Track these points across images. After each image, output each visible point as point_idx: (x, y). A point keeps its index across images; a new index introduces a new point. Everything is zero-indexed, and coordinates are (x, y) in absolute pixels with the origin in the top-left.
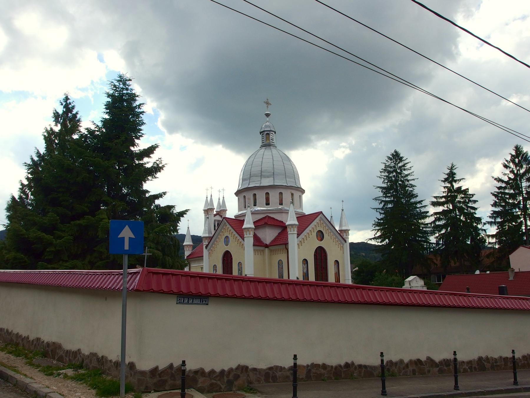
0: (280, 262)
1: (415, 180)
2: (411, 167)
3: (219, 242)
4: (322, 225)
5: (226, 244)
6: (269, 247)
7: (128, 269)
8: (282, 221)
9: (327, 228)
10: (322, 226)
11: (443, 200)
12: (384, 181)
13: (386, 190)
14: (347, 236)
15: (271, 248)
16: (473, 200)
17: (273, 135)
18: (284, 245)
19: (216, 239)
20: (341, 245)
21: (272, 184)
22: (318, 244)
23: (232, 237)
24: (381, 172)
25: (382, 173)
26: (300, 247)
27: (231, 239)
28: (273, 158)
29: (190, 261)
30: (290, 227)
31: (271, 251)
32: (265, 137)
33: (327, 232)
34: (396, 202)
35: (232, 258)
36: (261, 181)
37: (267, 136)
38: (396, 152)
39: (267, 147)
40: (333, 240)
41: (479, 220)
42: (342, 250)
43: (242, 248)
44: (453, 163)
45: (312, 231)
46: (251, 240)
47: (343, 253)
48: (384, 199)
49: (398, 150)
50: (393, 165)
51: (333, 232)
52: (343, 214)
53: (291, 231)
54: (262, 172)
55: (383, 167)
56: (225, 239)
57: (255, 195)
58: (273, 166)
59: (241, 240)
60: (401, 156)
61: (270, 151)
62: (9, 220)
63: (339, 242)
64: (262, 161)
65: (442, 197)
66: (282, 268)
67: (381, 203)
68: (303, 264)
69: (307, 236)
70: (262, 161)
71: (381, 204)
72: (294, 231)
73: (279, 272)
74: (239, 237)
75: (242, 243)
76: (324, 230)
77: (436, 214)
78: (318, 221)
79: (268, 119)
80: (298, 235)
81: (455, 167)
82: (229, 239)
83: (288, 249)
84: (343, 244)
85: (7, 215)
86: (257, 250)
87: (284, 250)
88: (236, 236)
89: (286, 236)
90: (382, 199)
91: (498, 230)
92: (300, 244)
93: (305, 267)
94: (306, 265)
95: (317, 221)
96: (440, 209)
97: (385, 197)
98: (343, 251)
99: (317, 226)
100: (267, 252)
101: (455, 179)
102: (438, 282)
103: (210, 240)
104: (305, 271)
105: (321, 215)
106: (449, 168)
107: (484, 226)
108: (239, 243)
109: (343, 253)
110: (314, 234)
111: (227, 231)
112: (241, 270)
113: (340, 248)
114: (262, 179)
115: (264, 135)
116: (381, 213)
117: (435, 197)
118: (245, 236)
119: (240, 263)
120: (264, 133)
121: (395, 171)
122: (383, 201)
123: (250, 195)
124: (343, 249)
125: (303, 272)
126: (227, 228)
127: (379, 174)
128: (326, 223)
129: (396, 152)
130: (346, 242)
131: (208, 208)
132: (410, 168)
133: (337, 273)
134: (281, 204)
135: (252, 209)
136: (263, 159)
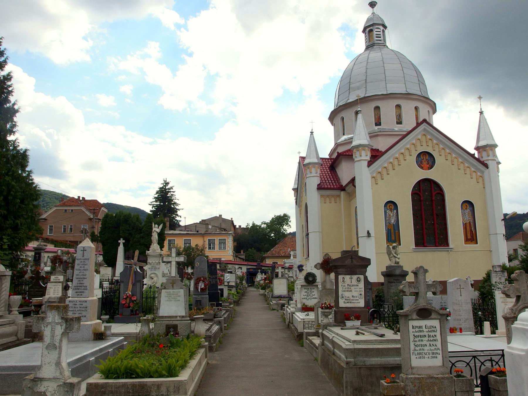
7: (400, 348)
14: (488, 156)
20: (479, 174)
26: (380, 182)
51: (455, 152)
54: (351, 84)
72: (361, 156)
80: (370, 164)
84: (483, 172)
85: (314, 284)
93: (392, 215)
94: (395, 211)
95: (417, 135)
104: (392, 222)
105: (425, 125)
109: (484, 188)
124: (483, 180)
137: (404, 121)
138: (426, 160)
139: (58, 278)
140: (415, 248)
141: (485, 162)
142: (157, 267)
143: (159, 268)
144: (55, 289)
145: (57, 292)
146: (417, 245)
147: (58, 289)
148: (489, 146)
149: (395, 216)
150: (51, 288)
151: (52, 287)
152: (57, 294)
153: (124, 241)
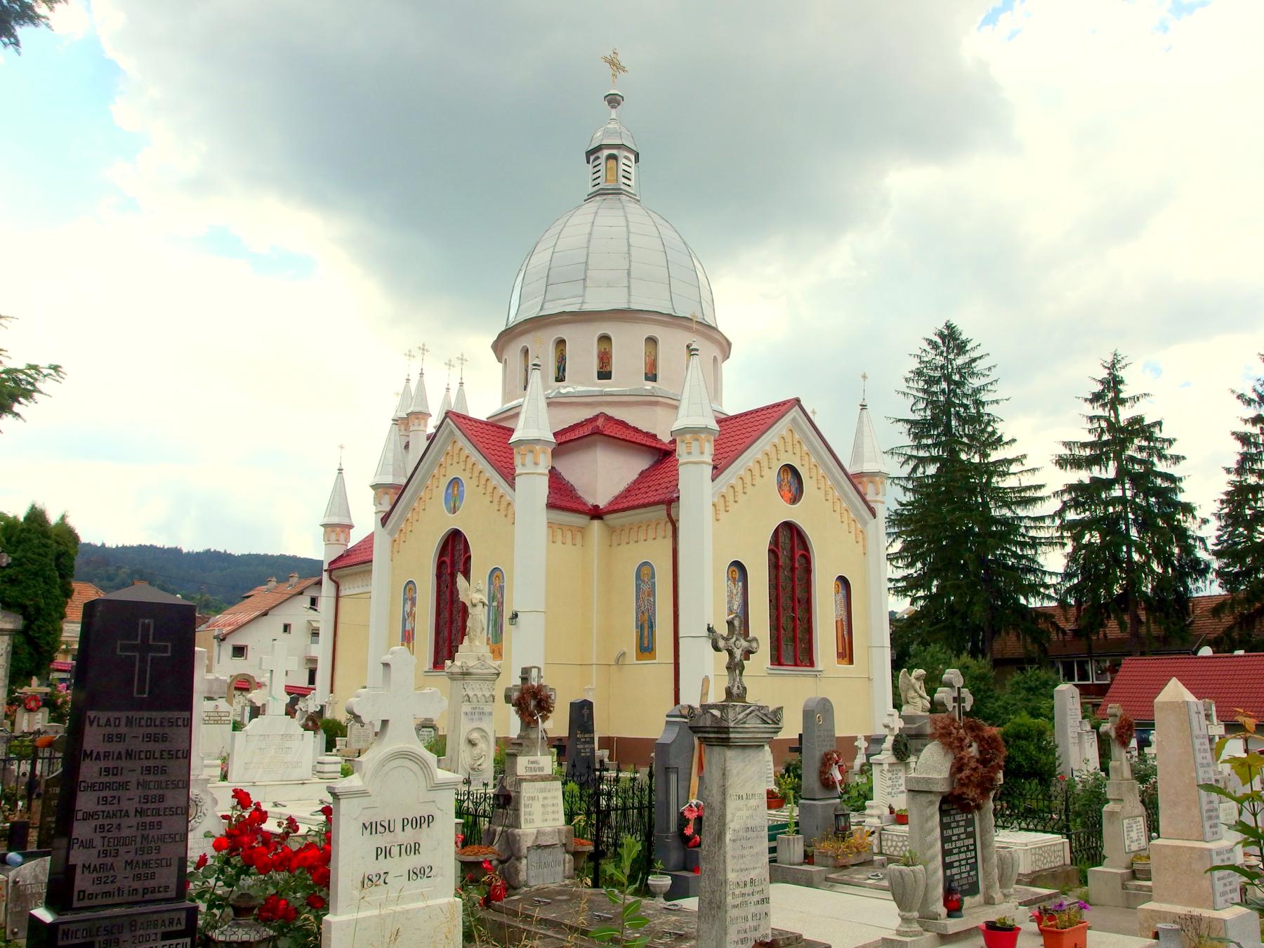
0: (645, 570)
1: (1001, 403)
2: (990, 369)
3: (428, 500)
4: (798, 446)
5: (452, 505)
6: (607, 517)
8: (653, 432)
9: (813, 460)
10: (797, 450)
11: (1088, 452)
12: (914, 404)
13: (919, 429)
15: (611, 519)
16: (1171, 456)
17: (629, 163)
18: (664, 507)
19: (416, 492)
21: (622, 305)
22: (788, 513)
23: (475, 482)
24: (907, 380)
25: (911, 382)
26: (722, 515)
27: (468, 486)
28: (627, 226)
29: (338, 577)
30: (688, 436)
31: (612, 530)
32: (602, 167)
33: (814, 474)
34: (950, 464)
35: (469, 557)
36: (583, 296)
37: (612, 163)
38: (948, 327)
39: (610, 196)
41: (1188, 509)
42: (861, 543)
43: (506, 516)
44: (1118, 352)
45: (765, 464)
46: (542, 487)
47: (865, 554)
48: (915, 453)
49: (954, 322)
50: (940, 361)
52: (865, 419)
53: (689, 453)
55: (915, 364)
56: (450, 491)
57: (561, 343)
58: (629, 249)
59: (503, 486)
60: (963, 337)
61: (621, 213)
62: (27, 518)
63: (852, 516)
64: (590, 234)
65: (1084, 445)
66: (652, 593)
67: (906, 462)
68: (729, 580)
69: (748, 480)
70: (590, 234)
71: (905, 466)
73: (638, 607)
74: (497, 479)
75: (508, 498)
76: (803, 465)
77: (1070, 488)
78: (784, 433)
79: (614, 113)
80: (717, 470)
81: (1123, 363)
82: (461, 489)
83: (678, 520)
84: (865, 523)
87: (661, 527)
88: (487, 475)
89: (674, 473)
90: (909, 453)
91: (1219, 547)
92: (722, 505)
93: (735, 592)
94: (740, 584)
96: (1083, 476)
97: (918, 447)
98: (864, 546)
99: (781, 448)
100: (596, 534)
101: (1121, 396)
102: (1079, 680)
103: (396, 497)
104: (735, 607)
105: (796, 411)
106: (1105, 364)
107: (1204, 527)
108: (496, 499)
109: (865, 554)
110: (772, 476)
111: (455, 460)
112: (499, 596)
114: (588, 290)
115: (602, 160)
116: (905, 489)
117: (1067, 444)
118: (518, 472)
119: (498, 573)
120: (599, 154)
121: (948, 378)
122: (910, 457)
123: (542, 346)
126: (456, 451)
127: (903, 386)
128: (810, 443)
129: (948, 327)
130: (874, 515)
131: (409, 411)
132: (987, 373)
134: (652, 377)
135: (550, 391)
136: (595, 228)
137: (615, 368)
138: (788, 482)
140: (769, 666)
141: (872, 505)
142: (487, 709)
143: (491, 714)
145: (553, 812)
148: (867, 476)
149: (739, 594)
150: (533, 798)
151: (536, 794)
152: (554, 820)
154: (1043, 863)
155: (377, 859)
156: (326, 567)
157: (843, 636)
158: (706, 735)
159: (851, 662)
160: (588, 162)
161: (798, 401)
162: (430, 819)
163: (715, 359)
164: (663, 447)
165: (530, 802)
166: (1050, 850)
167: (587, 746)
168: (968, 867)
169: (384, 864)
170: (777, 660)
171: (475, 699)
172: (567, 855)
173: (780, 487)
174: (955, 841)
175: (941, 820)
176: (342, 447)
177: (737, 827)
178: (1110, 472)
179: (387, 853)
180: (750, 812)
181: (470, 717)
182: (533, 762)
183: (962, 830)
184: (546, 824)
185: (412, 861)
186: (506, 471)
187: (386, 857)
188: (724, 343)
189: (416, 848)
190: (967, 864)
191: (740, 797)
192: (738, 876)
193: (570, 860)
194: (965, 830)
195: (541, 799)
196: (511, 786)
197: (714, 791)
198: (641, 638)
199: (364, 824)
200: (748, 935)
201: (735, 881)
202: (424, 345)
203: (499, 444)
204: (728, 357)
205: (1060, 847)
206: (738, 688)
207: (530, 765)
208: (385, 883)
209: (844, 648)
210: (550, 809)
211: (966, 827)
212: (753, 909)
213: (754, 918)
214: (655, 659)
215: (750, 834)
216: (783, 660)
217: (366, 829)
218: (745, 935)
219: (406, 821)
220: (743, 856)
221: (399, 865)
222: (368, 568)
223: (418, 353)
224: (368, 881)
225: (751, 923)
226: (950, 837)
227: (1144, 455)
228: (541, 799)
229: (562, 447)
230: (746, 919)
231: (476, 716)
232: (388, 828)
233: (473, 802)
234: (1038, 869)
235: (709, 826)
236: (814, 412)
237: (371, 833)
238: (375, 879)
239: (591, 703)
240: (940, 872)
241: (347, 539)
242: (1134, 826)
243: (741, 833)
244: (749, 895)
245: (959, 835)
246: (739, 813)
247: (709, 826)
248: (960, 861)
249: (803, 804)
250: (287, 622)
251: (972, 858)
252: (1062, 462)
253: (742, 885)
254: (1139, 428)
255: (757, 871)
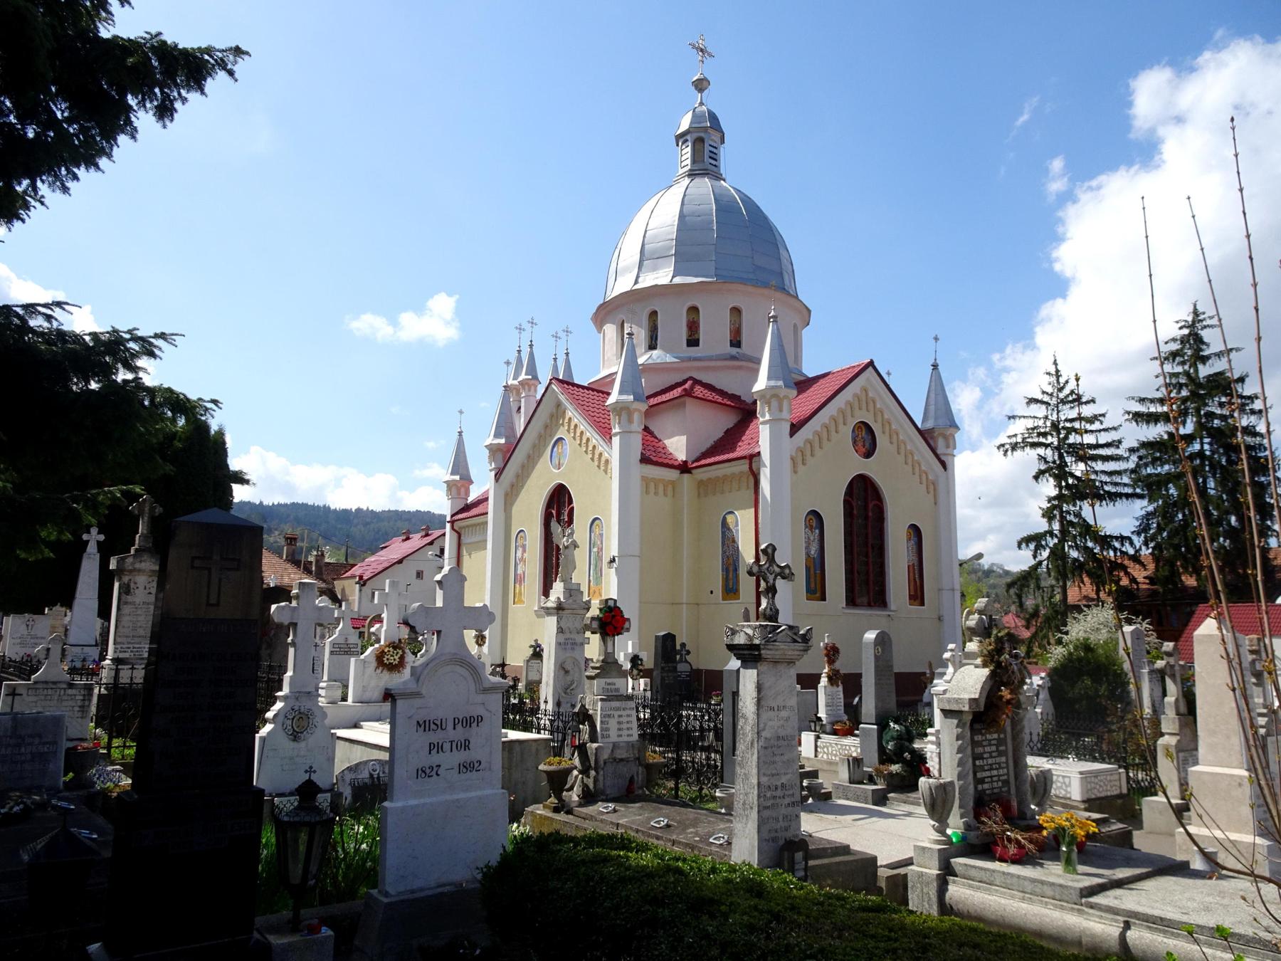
6: (694, 471)
14: (948, 447)
22: (858, 465)
26: (801, 468)
29: (460, 528)
40: (903, 457)
42: (932, 492)
47: (935, 504)
68: (806, 527)
73: (724, 552)
77: (1145, 445)
82: (564, 447)
86: (656, 482)
93: (812, 538)
94: (817, 531)
96: (1158, 431)
104: (813, 552)
109: (935, 504)
110: (847, 431)
112: (599, 543)
113: (924, 486)
119: (597, 522)
124: (935, 490)
125: (808, 555)
133: (914, 569)
139: (615, 684)
141: (943, 458)
144: (621, 719)
146: (847, 604)
147: (629, 719)
152: (628, 735)
153: (102, 537)
154: (1098, 790)
155: (430, 753)
156: (448, 519)
157: (915, 579)
158: (741, 652)
159: (922, 604)
160: (678, 145)
161: (871, 364)
162: (480, 719)
163: (795, 326)
164: (747, 407)
165: (607, 719)
166: (1106, 779)
167: (670, 674)
168: (1000, 784)
169: (436, 758)
170: (852, 601)
171: (567, 631)
172: (640, 768)
173: (855, 442)
174: (987, 758)
175: (972, 739)
176: (461, 412)
177: (768, 735)
178: (1189, 428)
179: (440, 748)
180: (782, 722)
181: (563, 647)
182: (609, 684)
183: (994, 748)
184: (621, 739)
185: (462, 756)
186: (604, 430)
187: (438, 752)
188: (805, 311)
189: (466, 745)
190: (999, 780)
191: (772, 709)
192: (769, 780)
193: (643, 772)
194: (997, 748)
195: (616, 716)
196: (589, 705)
197: (748, 703)
198: (726, 580)
199: (418, 722)
200: (779, 835)
201: (766, 784)
202: (532, 319)
203: (598, 403)
204: (808, 324)
205: (1116, 777)
206: (771, 609)
207: (607, 687)
208: (437, 775)
209: (916, 591)
210: (625, 726)
211: (997, 746)
212: (783, 811)
213: (785, 820)
214: (739, 599)
215: (781, 743)
216: (858, 601)
217: (420, 726)
218: (776, 834)
219: (457, 721)
220: (774, 763)
221: (450, 759)
222: (484, 520)
223: (527, 326)
224: (425, 773)
225: (782, 824)
226: (982, 754)
227: (1226, 412)
228: (616, 716)
229: (652, 409)
230: (777, 820)
231: (569, 646)
232: (439, 725)
233: (562, 721)
234: (1093, 797)
235: (743, 734)
236: (889, 374)
237: (425, 730)
238: (428, 771)
239: (674, 636)
240: (972, 787)
241: (467, 493)
242: (1190, 759)
243: (772, 741)
244: (780, 797)
245: (990, 753)
246: (770, 723)
247: (743, 734)
248: (991, 777)
249: (863, 728)
250: (420, 569)
251: (1003, 775)
252: (1138, 417)
253: (774, 788)
254: (1222, 385)
255: (788, 777)
